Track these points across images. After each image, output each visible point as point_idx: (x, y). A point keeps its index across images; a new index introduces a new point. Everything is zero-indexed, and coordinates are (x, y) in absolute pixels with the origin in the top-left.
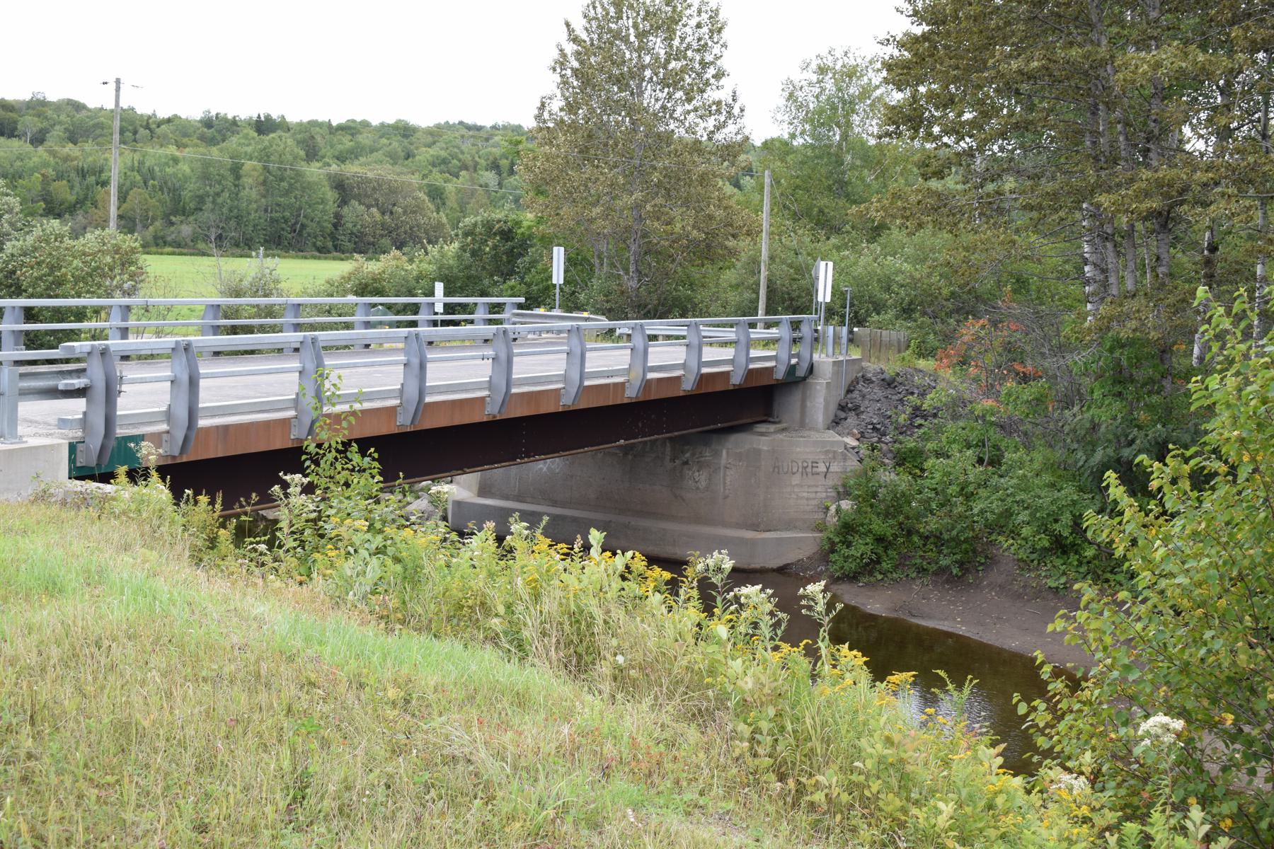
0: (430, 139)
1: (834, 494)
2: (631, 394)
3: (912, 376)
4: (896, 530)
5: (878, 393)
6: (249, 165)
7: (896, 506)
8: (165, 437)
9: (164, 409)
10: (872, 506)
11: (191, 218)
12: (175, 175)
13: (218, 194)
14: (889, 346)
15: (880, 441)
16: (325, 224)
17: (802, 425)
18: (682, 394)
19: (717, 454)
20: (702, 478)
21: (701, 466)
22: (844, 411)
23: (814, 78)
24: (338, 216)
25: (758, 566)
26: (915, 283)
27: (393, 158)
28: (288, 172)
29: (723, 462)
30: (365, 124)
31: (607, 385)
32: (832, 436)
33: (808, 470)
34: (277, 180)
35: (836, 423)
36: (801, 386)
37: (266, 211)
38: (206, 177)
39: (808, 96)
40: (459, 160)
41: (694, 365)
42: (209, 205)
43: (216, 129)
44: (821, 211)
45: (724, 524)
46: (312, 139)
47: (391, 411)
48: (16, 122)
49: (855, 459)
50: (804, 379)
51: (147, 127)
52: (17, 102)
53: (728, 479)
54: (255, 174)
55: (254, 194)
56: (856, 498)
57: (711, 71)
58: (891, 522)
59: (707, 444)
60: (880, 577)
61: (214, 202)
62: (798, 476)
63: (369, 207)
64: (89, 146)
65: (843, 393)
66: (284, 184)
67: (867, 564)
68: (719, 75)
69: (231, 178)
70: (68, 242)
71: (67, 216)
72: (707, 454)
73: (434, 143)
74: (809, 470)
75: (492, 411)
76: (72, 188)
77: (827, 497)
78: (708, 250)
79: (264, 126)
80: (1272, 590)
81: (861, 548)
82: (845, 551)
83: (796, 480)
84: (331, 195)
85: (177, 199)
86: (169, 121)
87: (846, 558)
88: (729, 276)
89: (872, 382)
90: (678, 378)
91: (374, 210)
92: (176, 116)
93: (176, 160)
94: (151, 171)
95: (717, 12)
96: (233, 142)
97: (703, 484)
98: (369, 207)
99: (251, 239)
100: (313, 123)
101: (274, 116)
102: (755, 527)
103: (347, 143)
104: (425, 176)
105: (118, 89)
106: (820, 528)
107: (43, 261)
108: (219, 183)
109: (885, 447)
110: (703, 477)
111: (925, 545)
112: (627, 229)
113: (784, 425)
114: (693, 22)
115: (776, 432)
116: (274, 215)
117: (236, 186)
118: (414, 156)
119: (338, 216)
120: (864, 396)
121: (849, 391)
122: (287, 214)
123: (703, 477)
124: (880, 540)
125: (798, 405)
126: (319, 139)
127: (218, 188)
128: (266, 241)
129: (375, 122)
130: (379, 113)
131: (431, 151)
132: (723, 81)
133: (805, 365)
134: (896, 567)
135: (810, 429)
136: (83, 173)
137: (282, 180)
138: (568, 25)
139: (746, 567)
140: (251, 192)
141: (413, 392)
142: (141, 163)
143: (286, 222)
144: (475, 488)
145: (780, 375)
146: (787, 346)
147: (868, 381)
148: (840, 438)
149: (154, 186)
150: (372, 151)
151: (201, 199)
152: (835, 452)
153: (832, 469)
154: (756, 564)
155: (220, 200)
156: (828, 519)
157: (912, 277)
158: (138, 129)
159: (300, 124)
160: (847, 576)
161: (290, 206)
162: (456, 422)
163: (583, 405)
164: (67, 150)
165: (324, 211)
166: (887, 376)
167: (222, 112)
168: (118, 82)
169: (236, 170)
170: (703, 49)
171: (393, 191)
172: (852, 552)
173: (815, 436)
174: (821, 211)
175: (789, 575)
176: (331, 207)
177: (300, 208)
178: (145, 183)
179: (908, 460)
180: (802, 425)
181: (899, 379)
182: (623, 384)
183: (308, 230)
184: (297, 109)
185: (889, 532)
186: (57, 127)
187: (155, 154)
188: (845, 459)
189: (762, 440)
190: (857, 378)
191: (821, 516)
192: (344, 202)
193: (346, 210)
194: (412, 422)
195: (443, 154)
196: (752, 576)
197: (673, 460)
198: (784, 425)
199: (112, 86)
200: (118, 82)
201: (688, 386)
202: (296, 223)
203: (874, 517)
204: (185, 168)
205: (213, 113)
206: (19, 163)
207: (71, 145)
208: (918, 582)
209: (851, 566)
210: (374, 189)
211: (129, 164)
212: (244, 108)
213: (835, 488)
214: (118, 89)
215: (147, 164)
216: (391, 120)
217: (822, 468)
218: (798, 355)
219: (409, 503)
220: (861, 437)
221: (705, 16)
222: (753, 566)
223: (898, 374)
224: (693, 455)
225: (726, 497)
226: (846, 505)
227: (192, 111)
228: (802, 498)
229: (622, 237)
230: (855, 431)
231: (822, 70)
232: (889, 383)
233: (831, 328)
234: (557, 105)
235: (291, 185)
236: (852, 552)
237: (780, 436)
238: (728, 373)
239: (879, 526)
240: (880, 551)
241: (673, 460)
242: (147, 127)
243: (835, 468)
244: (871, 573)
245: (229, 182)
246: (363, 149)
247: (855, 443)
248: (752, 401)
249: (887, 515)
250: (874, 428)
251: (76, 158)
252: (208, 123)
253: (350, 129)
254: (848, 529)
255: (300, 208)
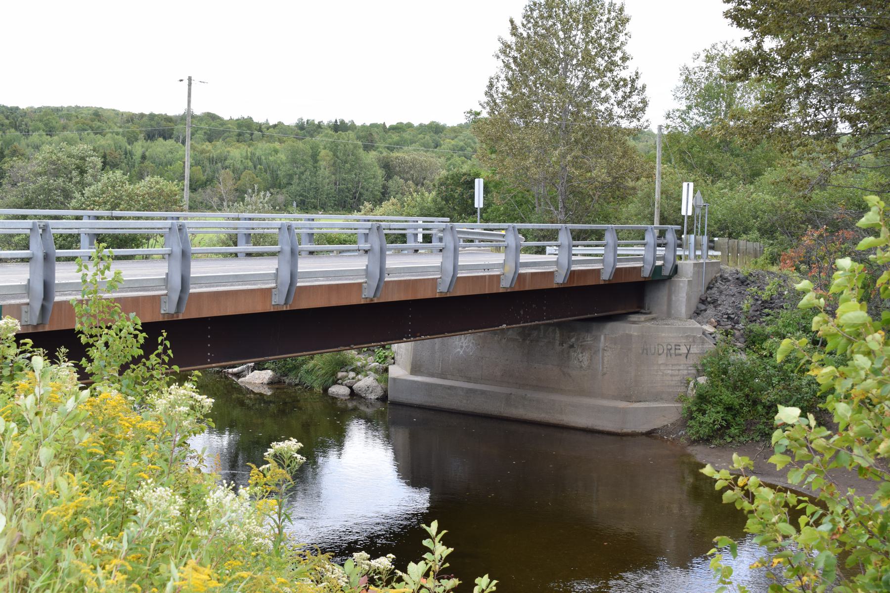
0: (453, 135)
1: (694, 372)
2: (505, 284)
3: (764, 276)
4: (742, 400)
5: (734, 289)
6: (323, 153)
7: (742, 380)
8: (24, 308)
9: (25, 283)
10: (722, 380)
11: (284, 190)
12: (275, 162)
13: (302, 173)
14: (746, 253)
15: (733, 328)
16: (377, 193)
17: (669, 315)
18: (555, 286)
19: (596, 339)
20: (585, 358)
21: (584, 349)
22: (704, 304)
23: (704, 65)
24: (385, 187)
25: (629, 431)
26: (774, 209)
27: (426, 146)
28: (351, 157)
29: (602, 345)
30: (409, 126)
31: (484, 277)
32: (694, 324)
33: (672, 351)
34: (343, 161)
35: (697, 313)
36: (667, 283)
37: (335, 184)
38: (294, 161)
39: (701, 77)
40: (472, 148)
41: (565, 262)
42: (296, 180)
43: (307, 129)
44: (711, 163)
45: (603, 396)
46: (370, 136)
47: (266, 293)
48: (173, 129)
49: (712, 342)
50: (670, 277)
51: (260, 130)
52: (176, 116)
53: (606, 359)
54: (328, 158)
55: (327, 173)
56: (709, 374)
57: (619, 54)
58: (738, 393)
59: (588, 331)
60: (729, 440)
61: (299, 178)
62: (663, 357)
63: (406, 180)
64: (219, 143)
65: (703, 289)
66: (348, 166)
67: (718, 429)
68: (624, 59)
69: (311, 162)
70: (128, 187)
71: (200, 190)
72: (589, 339)
73: (456, 137)
74: (673, 351)
75: (367, 295)
76: (204, 172)
77: (689, 374)
78: (617, 191)
79: (339, 127)
80: (441, 589)
81: (713, 415)
82: (701, 418)
83: (662, 360)
84: (380, 172)
85: (275, 177)
86: (275, 126)
87: (701, 423)
88: (632, 208)
89: (729, 281)
90: (552, 273)
91: (410, 182)
92: (280, 123)
93: (276, 151)
94: (259, 159)
95: (621, 10)
96: (318, 138)
97: (586, 363)
98: (406, 180)
99: (325, 203)
100: (373, 126)
101: (347, 121)
102: (628, 399)
103: (395, 137)
104: (449, 159)
105: (190, 85)
106: (680, 400)
107: (108, 201)
108: (303, 165)
109: (737, 333)
110: (585, 358)
111: (768, 413)
112: (555, 174)
113: (653, 316)
114: (605, 18)
115: (646, 321)
116: (342, 186)
117: (315, 167)
118: (441, 146)
119: (385, 187)
120: (721, 292)
121: (709, 288)
122: (350, 186)
123: (585, 358)
124: (729, 409)
125: (665, 298)
126: (375, 136)
127: (302, 169)
128: (335, 204)
129: (416, 124)
130: (419, 118)
131: (453, 142)
132: (628, 63)
133: (669, 266)
134: (744, 431)
135: (675, 319)
136: (212, 161)
137: (346, 162)
138: (512, 22)
139: (619, 431)
140: (325, 170)
141: (285, 276)
142: (253, 154)
143: (349, 191)
144: (409, 368)
145: (646, 273)
146: (652, 250)
147: (725, 280)
148: (699, 326)
149: (260, 169)
150: (412, 143)
151: (291, 177)
152: (694, 337)
153: (692, 351)
154: (628, 429)
155: (304, 177)
156: (689, 392)
157: (773, 205)
158: (247, 130)
159: (363, 126)
160: (702, 439)
161: (352, 181)
162: (334, 303)
163: (459, 293)
164: (204, 147)
165: (375, 184)
166: (741, 276)
167: (311, 118)
168: (190, 79)
169: (315, 157)
170: (613, 38)
171: (423, 169)
172: (706, 419)
173: (678, 324)
174: (711, 163)
175: (656, 438)
176: (380, 181)
177: (359, 182)
178: (255, 168)
179: (753, 341)
180: (669, 315)
181: (752, 279)
182: (498, 276)
183: (365, 197)
184: (362, 116)
185: (736, 402)
186: (199, 132)
187: (261, 148)
188: (703, 343)
189: (633, 328)
190: (716, 277)
191: (683, 389)
192: (389, 177)
193: (390, 182)
194: (286, 304)
195: (462, 144)
196: (624, 438)
197: (561, 344)
198: (653, 316)
199: (186, 82)
200: (190, 79)
201: (560, 279)
202: (355, 193)
203: (724, 389)
204: (282, 157)
205: (305, 120)
206: (169, 156)
207: (207, 143)
208: (761, 444)
209: (705, 431)
210: (410, 167)
211: (245, 154)
212: (325, 116)
213: (695, 366)
214: (190, 85)
215: (257, 154)
216: (426, 122)
217: (684, 350)
218: (663, 258)
219: (359, 380)
220: (718, 324)
221: (613, 14)
222: (625, 430)
223: (751, 275)
224: (577, 340)
225: (604, 374)
226: (702, 380)
227: (290, 121)
228: (666, 375)
229: (552, 179)
230: (713, 320)
231: (709, 59)
232: (743, 282)
233: (692, 236)
234: (502, 85)
235: (352, 165)
236: (706, 419)
237: (648, 324)
238: (599, 270)
239: (728, 397)
240: (729, 418)
241: (561, 344)
242: (260, 130)
243: (694, 350)
244: (722, 437)
245: (310, 165)
246: (405, 141)
247: (712, 330)
248: (629, 294)
249: (735, 388)
250: (729, 318)
251: (209, 151)
252: (301, 127)
253: (398, 128)
254: (703, 398)
255: (359, 182)
